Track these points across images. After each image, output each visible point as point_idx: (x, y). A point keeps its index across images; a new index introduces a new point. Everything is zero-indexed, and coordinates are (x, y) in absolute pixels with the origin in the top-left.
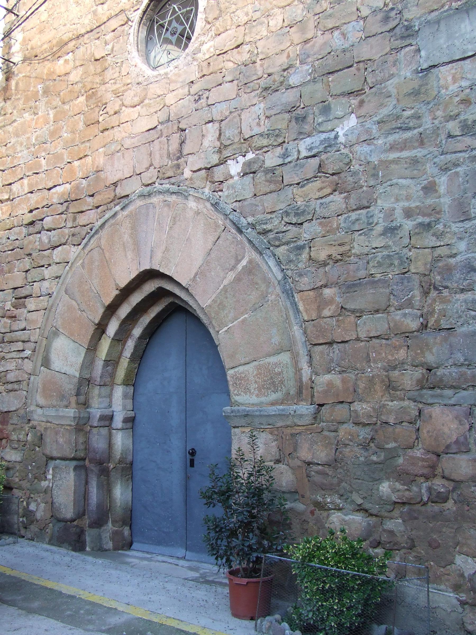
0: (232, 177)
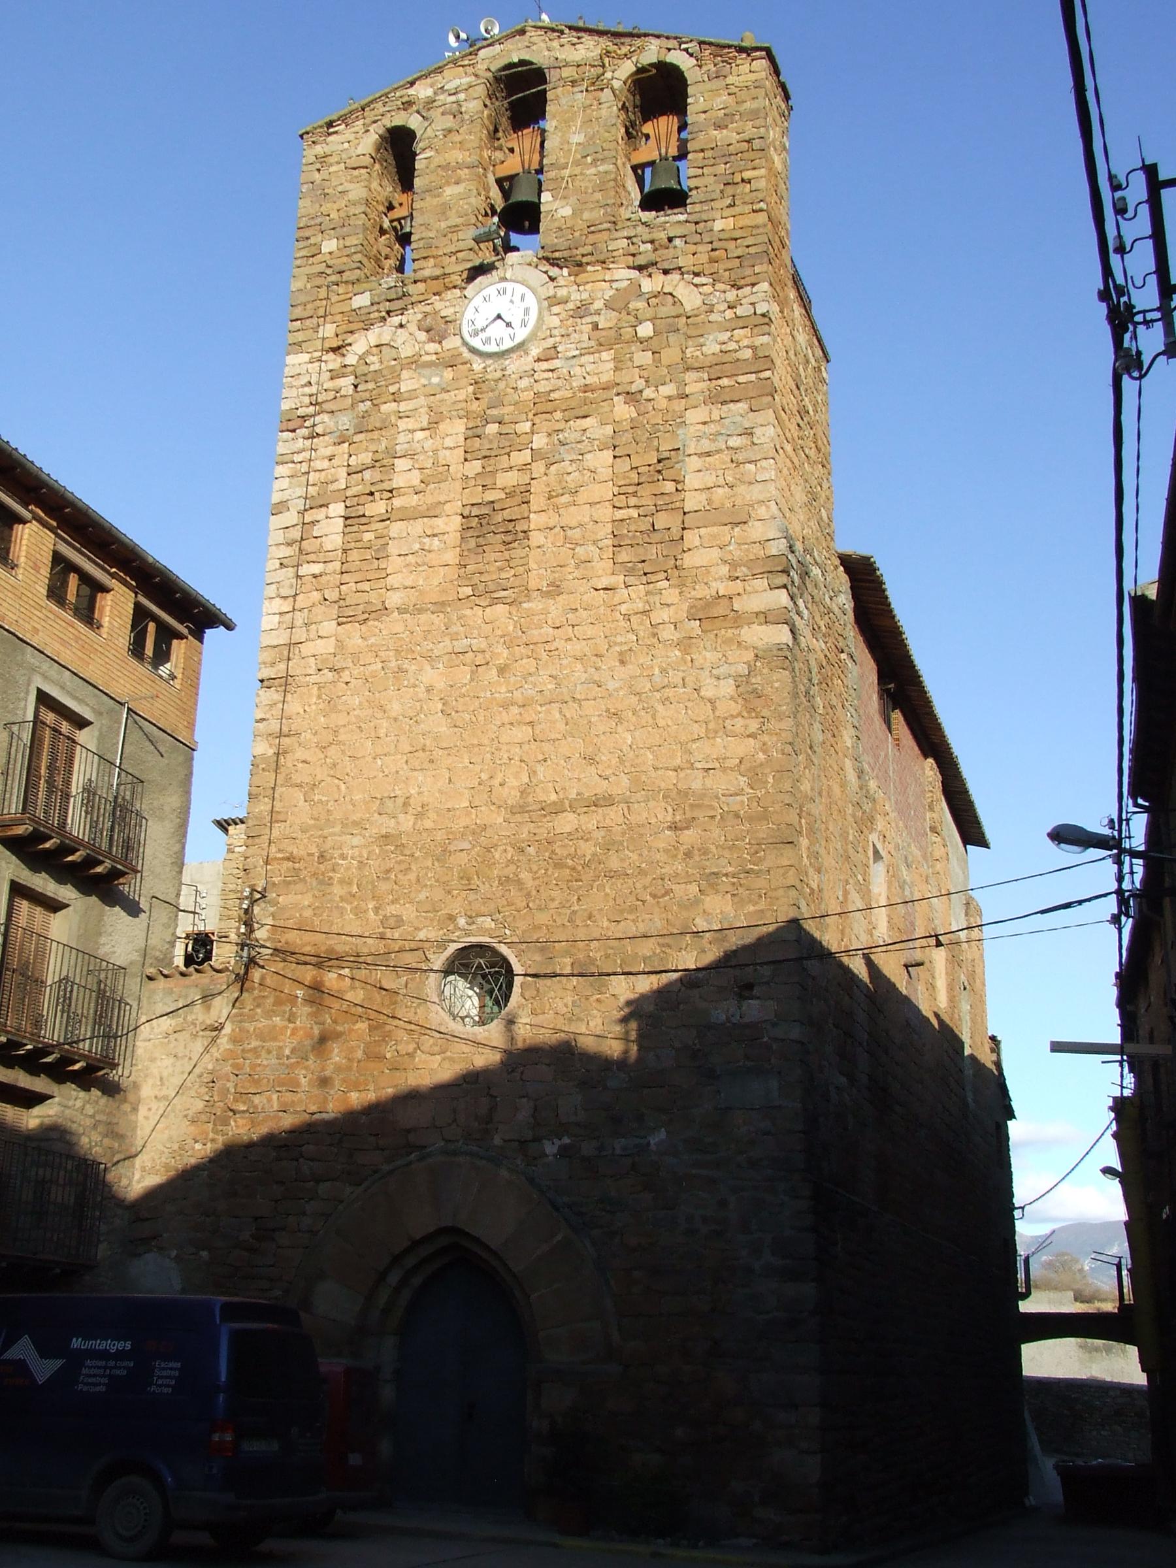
0: (547, 1156)
